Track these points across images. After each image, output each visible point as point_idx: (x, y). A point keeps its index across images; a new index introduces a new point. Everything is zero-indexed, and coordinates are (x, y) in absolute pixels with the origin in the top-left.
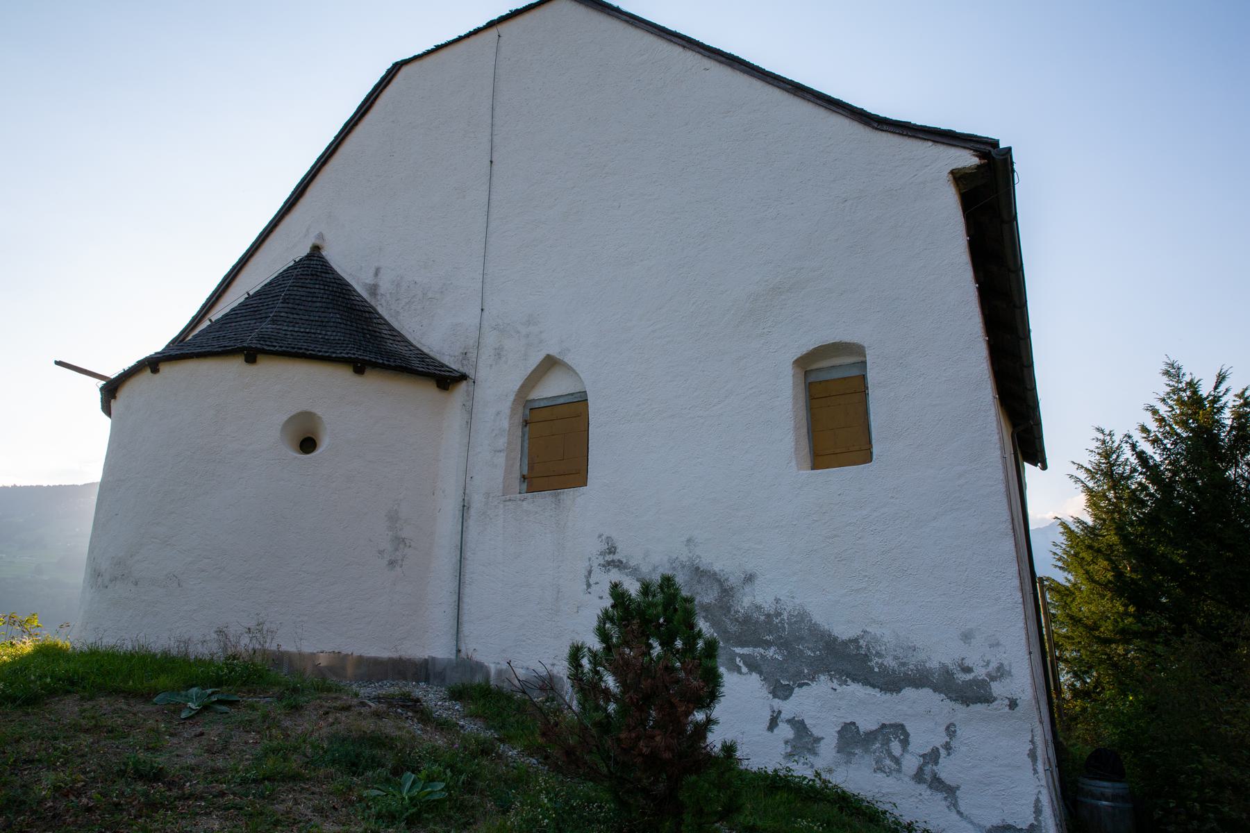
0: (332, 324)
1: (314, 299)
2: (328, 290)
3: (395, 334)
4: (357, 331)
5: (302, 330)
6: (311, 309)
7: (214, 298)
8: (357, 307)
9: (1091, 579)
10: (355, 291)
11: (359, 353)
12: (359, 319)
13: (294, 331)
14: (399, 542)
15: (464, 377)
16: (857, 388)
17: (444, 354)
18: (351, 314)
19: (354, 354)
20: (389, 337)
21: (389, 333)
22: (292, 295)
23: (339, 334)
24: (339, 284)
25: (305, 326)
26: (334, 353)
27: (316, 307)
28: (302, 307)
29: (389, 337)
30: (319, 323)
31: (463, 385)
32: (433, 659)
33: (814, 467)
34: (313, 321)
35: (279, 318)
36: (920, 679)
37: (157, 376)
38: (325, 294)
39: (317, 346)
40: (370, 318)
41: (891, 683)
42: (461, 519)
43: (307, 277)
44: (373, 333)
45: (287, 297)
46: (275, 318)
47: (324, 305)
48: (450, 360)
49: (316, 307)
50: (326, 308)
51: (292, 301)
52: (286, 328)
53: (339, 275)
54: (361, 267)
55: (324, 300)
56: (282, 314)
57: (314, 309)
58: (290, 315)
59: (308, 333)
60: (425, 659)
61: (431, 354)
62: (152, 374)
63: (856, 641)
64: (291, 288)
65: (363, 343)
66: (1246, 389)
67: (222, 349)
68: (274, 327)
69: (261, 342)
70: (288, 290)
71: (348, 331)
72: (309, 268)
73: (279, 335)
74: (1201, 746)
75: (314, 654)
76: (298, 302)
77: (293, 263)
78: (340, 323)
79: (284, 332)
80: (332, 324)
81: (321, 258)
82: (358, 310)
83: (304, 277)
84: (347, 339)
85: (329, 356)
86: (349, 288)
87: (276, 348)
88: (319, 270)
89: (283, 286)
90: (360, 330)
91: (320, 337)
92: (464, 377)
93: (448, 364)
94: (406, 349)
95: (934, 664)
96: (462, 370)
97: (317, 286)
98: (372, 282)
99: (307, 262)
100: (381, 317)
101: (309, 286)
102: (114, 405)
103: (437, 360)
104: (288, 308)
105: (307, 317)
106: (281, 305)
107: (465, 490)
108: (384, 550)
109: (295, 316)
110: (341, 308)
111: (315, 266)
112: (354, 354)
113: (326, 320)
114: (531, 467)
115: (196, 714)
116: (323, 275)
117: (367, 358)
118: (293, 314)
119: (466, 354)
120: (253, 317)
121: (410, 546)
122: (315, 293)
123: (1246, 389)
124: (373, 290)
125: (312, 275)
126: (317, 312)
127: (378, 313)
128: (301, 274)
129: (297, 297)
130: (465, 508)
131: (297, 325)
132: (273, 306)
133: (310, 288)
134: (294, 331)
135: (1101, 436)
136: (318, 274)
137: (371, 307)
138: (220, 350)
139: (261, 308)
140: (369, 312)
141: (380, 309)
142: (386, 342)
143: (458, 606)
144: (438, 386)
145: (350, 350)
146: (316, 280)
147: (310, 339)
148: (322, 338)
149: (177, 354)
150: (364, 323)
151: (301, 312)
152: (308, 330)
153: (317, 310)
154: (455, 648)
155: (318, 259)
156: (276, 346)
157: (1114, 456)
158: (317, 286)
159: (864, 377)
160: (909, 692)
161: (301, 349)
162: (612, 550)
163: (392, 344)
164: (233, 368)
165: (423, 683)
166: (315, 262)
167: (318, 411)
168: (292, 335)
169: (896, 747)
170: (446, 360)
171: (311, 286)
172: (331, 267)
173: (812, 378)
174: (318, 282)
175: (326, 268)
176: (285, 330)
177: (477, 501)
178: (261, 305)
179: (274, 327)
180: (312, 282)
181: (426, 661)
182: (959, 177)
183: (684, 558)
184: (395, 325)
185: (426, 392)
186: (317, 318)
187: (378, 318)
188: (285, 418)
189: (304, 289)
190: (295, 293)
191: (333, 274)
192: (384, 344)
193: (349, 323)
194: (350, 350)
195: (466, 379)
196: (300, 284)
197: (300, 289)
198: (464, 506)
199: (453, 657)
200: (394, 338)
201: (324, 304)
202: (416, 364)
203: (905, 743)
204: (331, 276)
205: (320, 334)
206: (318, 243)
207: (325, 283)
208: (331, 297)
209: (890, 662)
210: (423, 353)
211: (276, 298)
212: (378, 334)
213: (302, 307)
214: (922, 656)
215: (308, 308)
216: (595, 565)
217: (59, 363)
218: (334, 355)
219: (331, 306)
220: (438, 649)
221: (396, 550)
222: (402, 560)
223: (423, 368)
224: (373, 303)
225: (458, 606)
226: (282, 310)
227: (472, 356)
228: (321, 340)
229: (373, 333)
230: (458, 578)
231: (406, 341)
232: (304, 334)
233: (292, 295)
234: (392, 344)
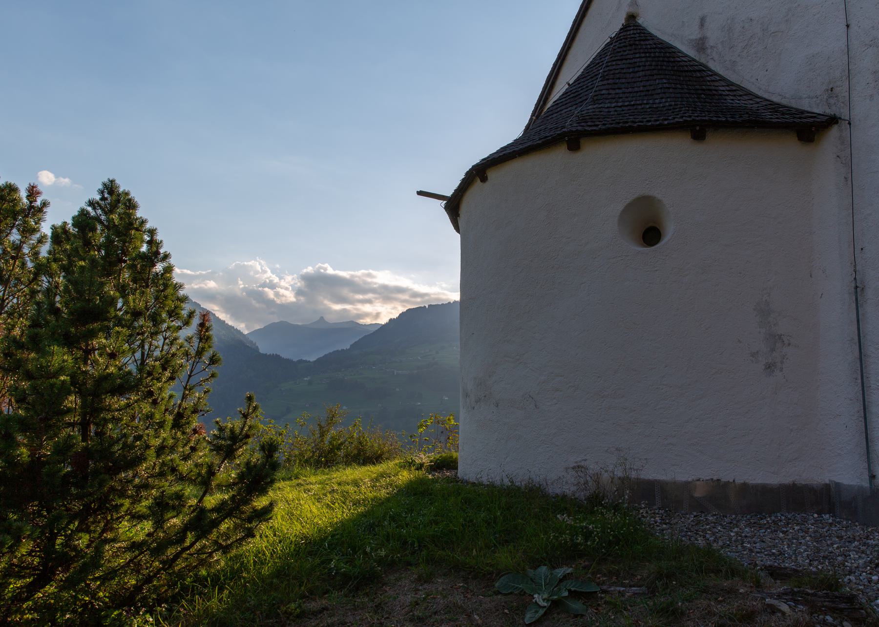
0: (659, 91)
1: (636, 69)
2: (649, 57)
3: (734, 88)
4: (689, 93)
5: (626, 104)
6: (633, 80)
7: (542, 103)
8: (686, 68)
10: (680, 52)
11: (696, 115)
12: (689, 81)
13: (618, 107)
14: (775, 340)
15: (833, 120)
17: (800, 98)
18: (680, 76)
19: (690, 117)
20: (727, 93)
21: (728, 88)
22: (612, 70)
23: (669, 100)
24: (662, 48)
25: (629, 99)
26: (666, 120)
27: (639, 77)
28: (624, 81)
29: (727, 93)
30: (644, 93)
31: (834, 131)
32: (838, 485)
34: (637, 92)
35: (599, 97)
37: (487, 185)
38: (648, 61)
39: (645, 116)
40: (702, 77)
42: (854, 305)
43: (625, 49)
44: (708, 92)
45: (605, 74)
46: (595, 98)
47: (649, 73)
49: (639, 77)
50: (651, 75)
51: (611, 76)
52: (609, 105)
53: (659, 39)
54: (683, 22)
55: (647, 68)
56: (604, 92)
57: (638, 79)
58: (612, 92)
59: (633, 105)
60: (826, 484)
61: (784, 102)
62: (482, 183)
64: (610, 64)
65: (699, 104)
67: (543, 140)
68: (595, 106)
69: (583, 124)
70: (607, 66)
71: (679, 95)
72: (626, 39)
73: (602, 113)
75: (690, 483)
76: (618, 76)
77: (609, 39)
78: (669, 88)
79: (607, 110)
80: (659, 91)
81: (638, 27)
82: (687, 71)
83: (621, 49)
84: (679, 103)
85: (660, 125)
86: (673, 50)
87: (599, 127)
88: (638, 39)
89: (600, 64)
90: (692, 91)
91: (648, 106)
92: (833, 120)
93: (809, 109)
94: (751, 102)
96: (828, 111)
97: (637, 55)
98: (699, 36)
99: (624, 33)
100: (715, 74)
101: (629, 57)
102: (461, 221)
103: (792, 108)
104: (608, 84)
105: (630, 90)
106: (601, 83)
107: (855, 266)
108: (757, 352)
109: (617, 91)
110: (667, 72)
111: (633, 36)
112: (690, 117)
113: (652, 88)
115: (545, 614)
116: (642, 43)
117: (707, 118)
118: (614, 89)
119: (832, 89)
120: (574, 103)
121: (789, 344)
122: (636, 62)
124: (701, 45)
125: (631, 45)
126: (641, 81)
127: (710, 70)
128: (619, 48)
129: (617, 71)
130: (858, 290)
131: (621, 100)
132: (592, 86)
133: (630, 59)
134: (618, 107)
136: (637, 42)
137: (701, 64)
138: (540, 142)
139: (582, 91)
140: (700, 71)
141: (712, 65)
142: (726, 99)
143: (865, 418)
144: (799, 140)
145: (684, 113)
146: (635, 49)
147: (637, 111)
148: (650, 108)
149: (500, 156)
150: (695, 83)
151: (623, 86)
152: (632, 103)
153: (640, 79)
154: (866, 472)
155: (635, 28)
156: (598, 125)
158: (637, 55)
161: (627, 122)
163: (733, 100)
164: (559, 156)
165: (828, 516)
166: (632, 32)
167: (657, 193)
168: (616, 111)
171: (631, 56)
172: (650, 33)
174: (637, 51)
176: (608, 107)
178: (580, 89)
179: (595, 106)
180: (630, 52)
181: (827, 487)
184: (733, 78)
186: (641, 88)
187: (712, 75)
188: (621, 207)
189: (624, 61)
190: (614, 67)
191: (653, 39)
192: (723, 101)
193: (679, 86)
194: (684, 113)
195: (837, 123)
196: (619, 58)
197: (619, 62)
198: (856, 287)
199: (866, 484)
200: (735, 93)
201: (647, 72)
202: (767, 116)
204: (651, 42)
205: (647, 104)
206: (632, 10)
207: (646, 50)
208: (654, 63)
210: (772, 103)
211: (595, 78)
212: (714, 92)
213: (624, 81)
215: (630, 80)
217: (420, 193)
218: (666, 122)
219: (655, 72)
221: (773, 350)
222: (782, 362)
223: (777, 118)
224: (703, 61)
225: (865, 418)
226: (602, 88)
228: (649, 110)
229: (708, 92)
230: (860, 381)
231: (749, 93)
232: (629, 107)
233: (612, 70)
234: (733, 100)
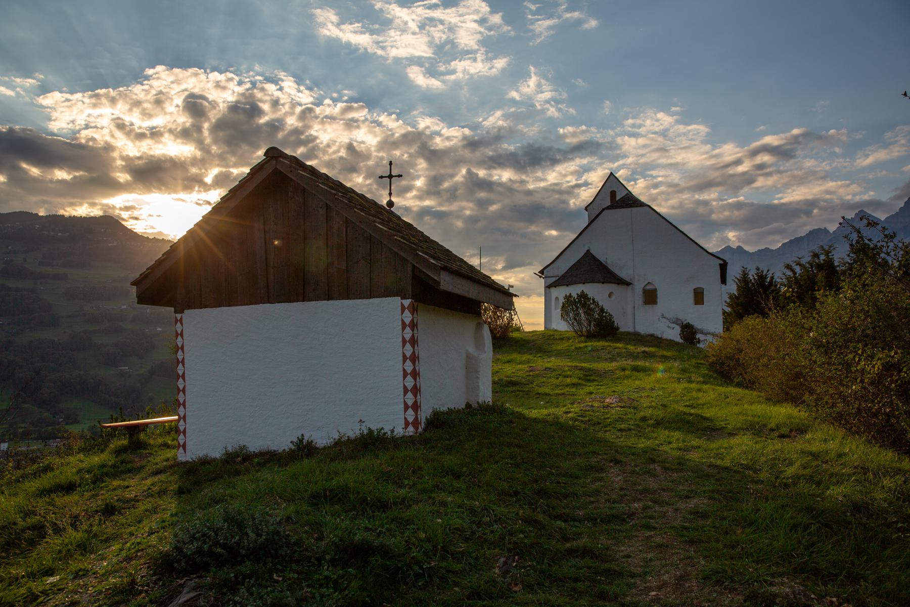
9: (735, 311)
14: (624, 313)
16: (702, 293)
36: (709, 334)
41: (706, 334)
48: (627, 279)
74: (318, 185)
92: (631, 284)
124: (606, 262)
170: (626, 280)
175: (594, 258)
182: (720, 264)
185: (625, 287)
220: (631, 330)
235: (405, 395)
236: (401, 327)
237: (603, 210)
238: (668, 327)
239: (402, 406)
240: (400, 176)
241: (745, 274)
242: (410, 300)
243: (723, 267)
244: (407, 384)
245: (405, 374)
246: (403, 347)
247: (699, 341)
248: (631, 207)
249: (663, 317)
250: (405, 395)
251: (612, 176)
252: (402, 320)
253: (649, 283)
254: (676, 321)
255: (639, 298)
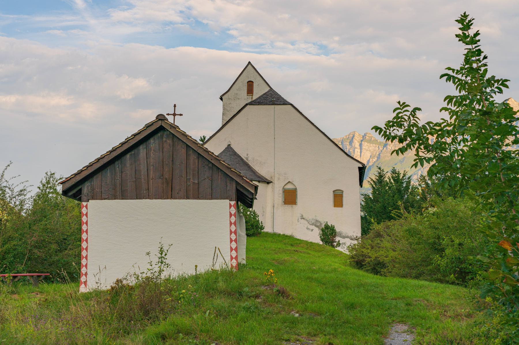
14: (263, 212)
33: (334, 207)
36: (347, 237)
41: (344, 237)
48: (269, 179)
63: (339, 232)
66: (473, 19)
95: (349, 235)
114: (285, 200)
123: (473, 19)
124: (247, 159)
135: (379, 171)
141: (249, 163)
157: (383, 178)
159: (342, 195)
160: (346, 239)
162: (302, 216)
169: (344, 246)
170: (267, 178)
173: (335, 193)
177: (276, 206)
182: (359, 168)
183: (315, 218)
203: (345, 245)
209: (344, 235)
214: (348, 234)
215: (226, 154)
216: (299, 218)
227: (273, 178)
235: (231, 252)
236: (229, 216)
237: (247, 105)
238: (308, 228)
239: (230, 257)
240: (181, 115)
241: (381, 176)
242: (234, 202)
243: (362, 170)
244: (232, 246)
245: (231, 241)
246: (230, 226)
247: (339, 244)
248: (274, 104)
249: (302, 218)
250: (231, 252)
251: (250, 65)
252: (230, 212)
253: (289, 182)
254: (316, 223)
255: (279, 198)
